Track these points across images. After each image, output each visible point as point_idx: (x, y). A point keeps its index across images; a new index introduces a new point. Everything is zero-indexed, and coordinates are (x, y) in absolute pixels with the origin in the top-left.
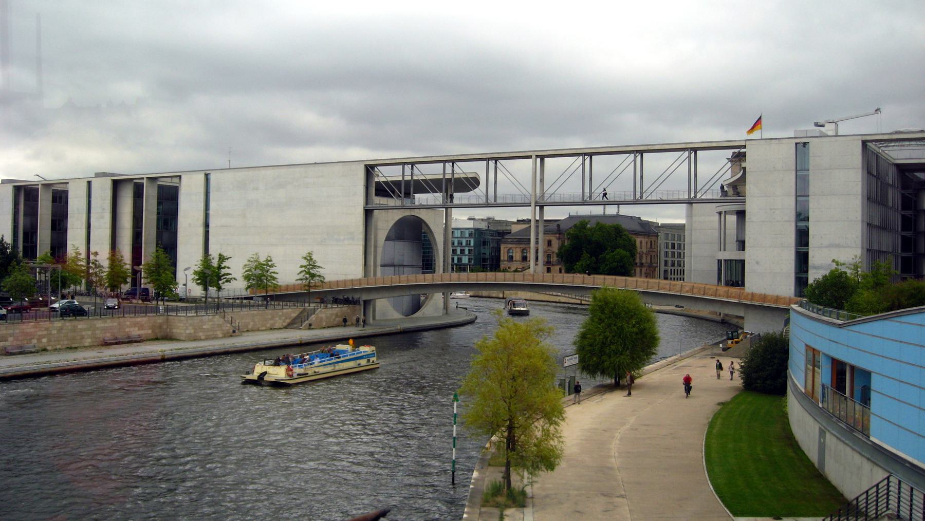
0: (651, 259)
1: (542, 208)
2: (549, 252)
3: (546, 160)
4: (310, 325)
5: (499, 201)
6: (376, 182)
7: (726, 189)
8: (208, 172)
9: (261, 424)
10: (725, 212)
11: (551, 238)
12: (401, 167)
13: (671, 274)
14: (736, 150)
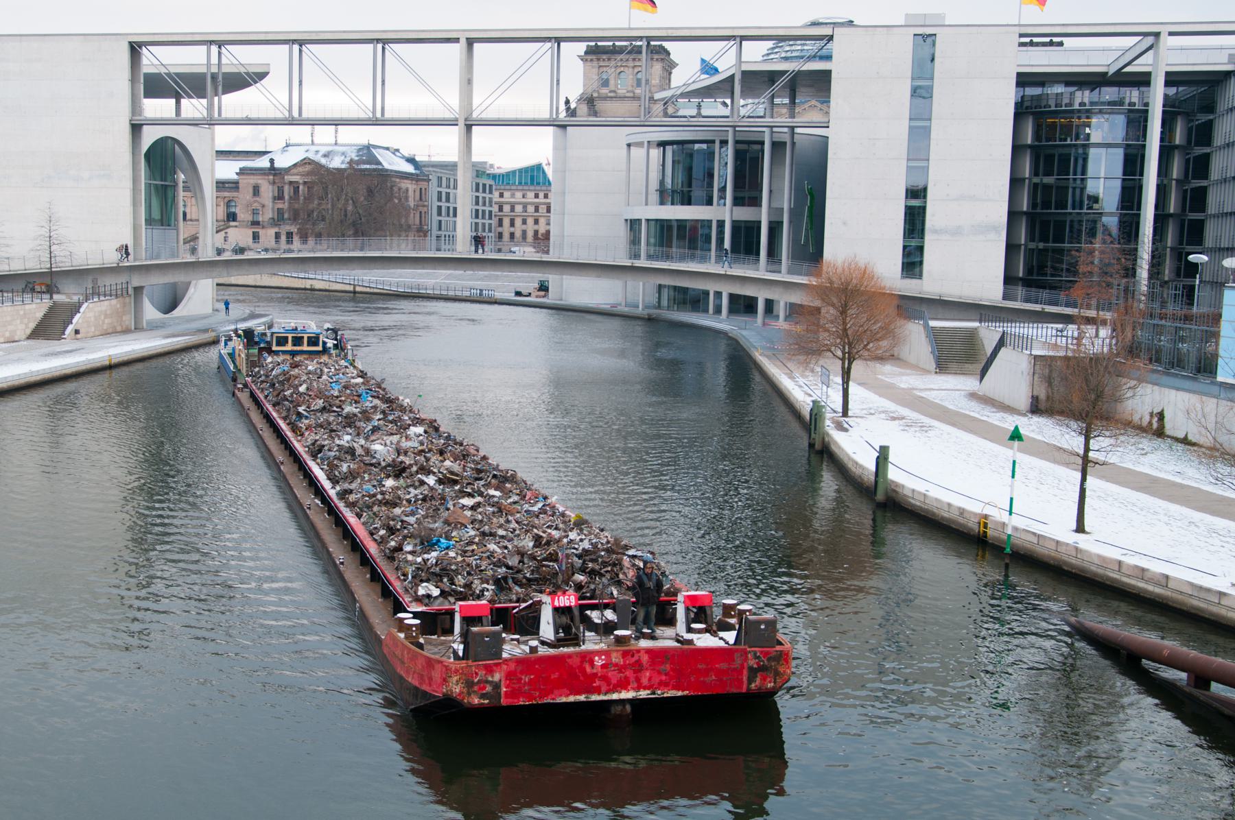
0: (421, 217)
1: (469, 128)
2: (256, 205)
3: (476, 46)
4: (77, 332)
5: (388, 115)
6: (145, 75)
9: (1207, 452)
10: (649, 142)
11: (260, 182)
12: (204, 48)
13: (445, 244)
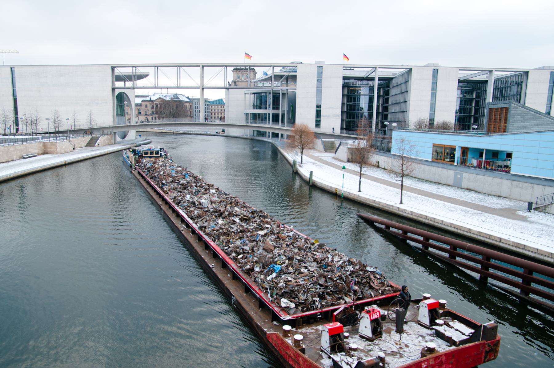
1: (203, 89)
2: (146, 110)
4: (99, 145)
6: (116, 75)
7: (230, 83)
8: (12, 67)
12: (132, 68)
14: (235, 67)
